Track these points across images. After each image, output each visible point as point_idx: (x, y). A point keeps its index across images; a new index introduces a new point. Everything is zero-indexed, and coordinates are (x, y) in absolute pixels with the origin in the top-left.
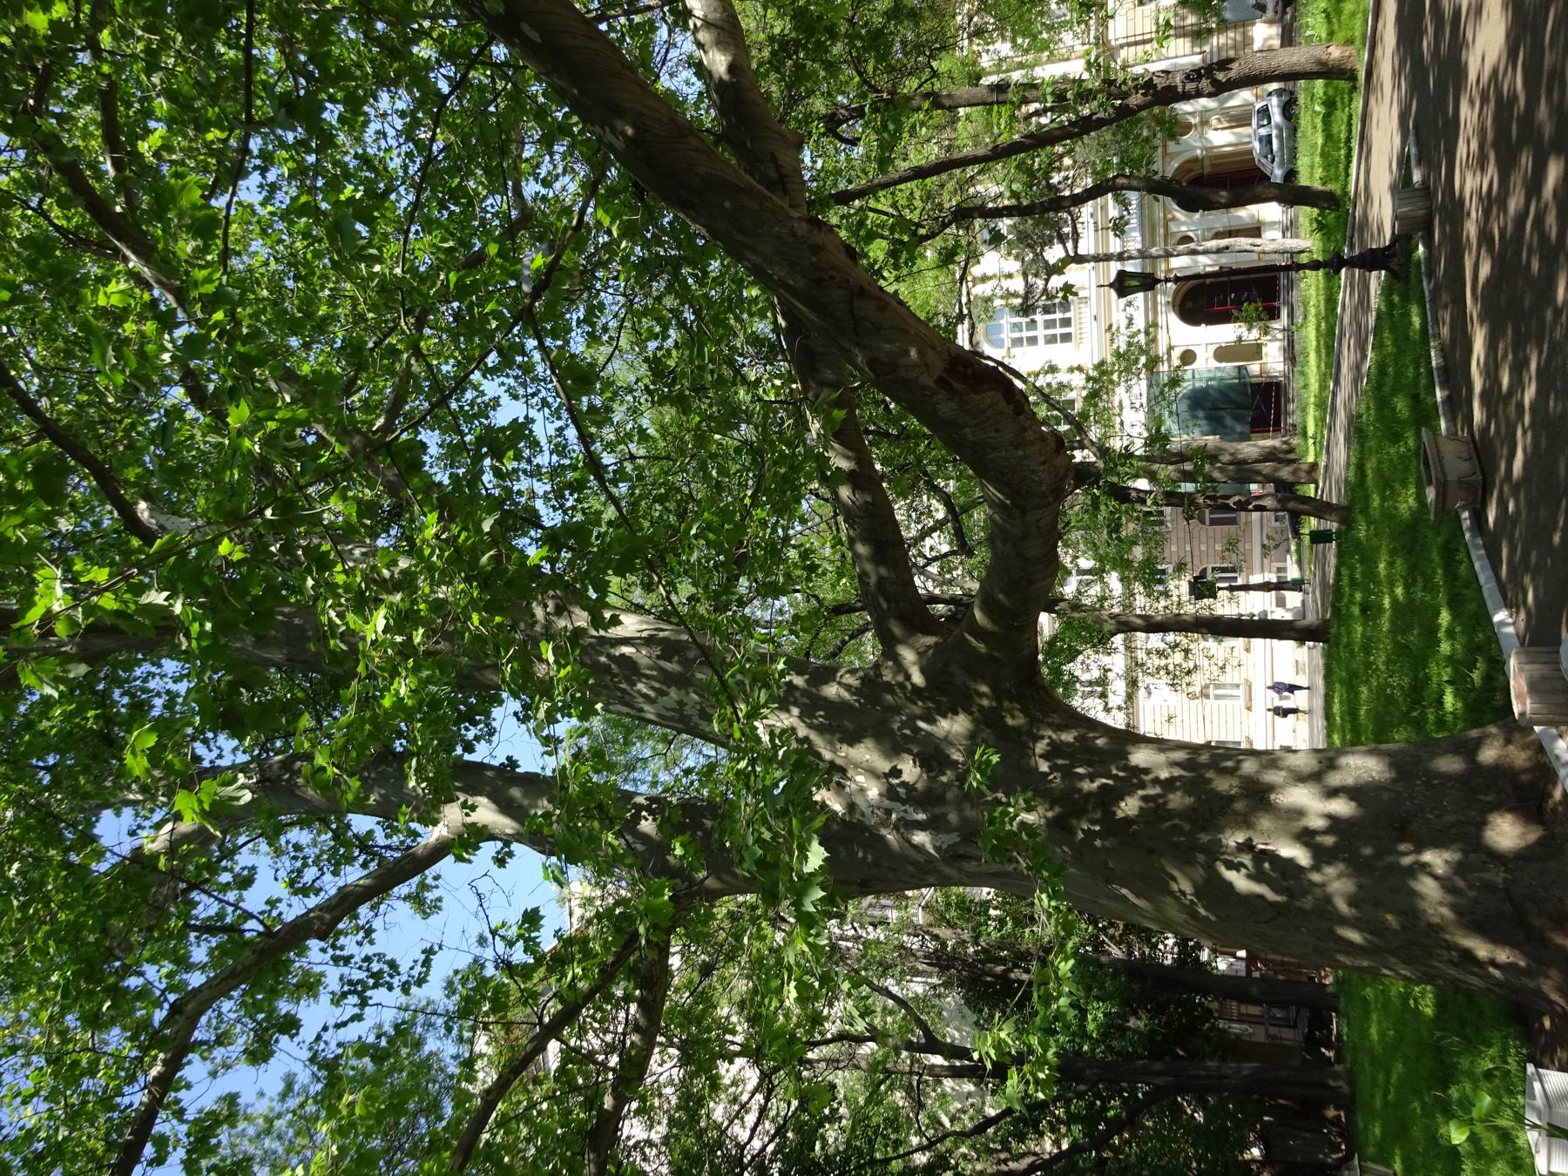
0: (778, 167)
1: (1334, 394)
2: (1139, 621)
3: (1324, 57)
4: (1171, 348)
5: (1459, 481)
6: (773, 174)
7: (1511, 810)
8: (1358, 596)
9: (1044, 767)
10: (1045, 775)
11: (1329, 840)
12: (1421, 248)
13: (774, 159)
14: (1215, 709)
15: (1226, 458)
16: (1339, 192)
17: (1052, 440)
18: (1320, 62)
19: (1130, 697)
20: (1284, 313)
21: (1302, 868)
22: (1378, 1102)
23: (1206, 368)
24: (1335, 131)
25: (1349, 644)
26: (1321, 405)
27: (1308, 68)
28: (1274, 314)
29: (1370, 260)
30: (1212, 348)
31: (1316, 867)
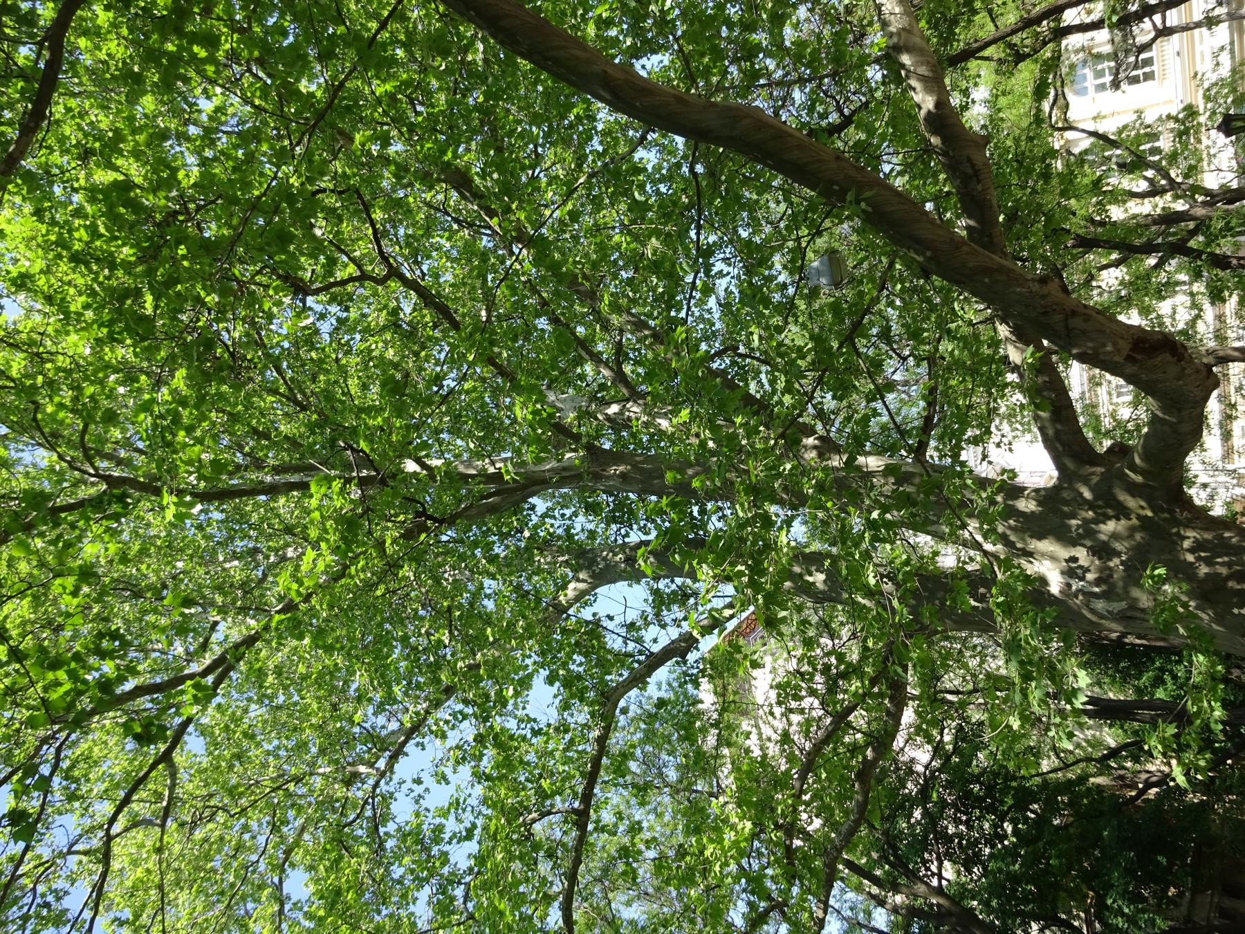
0: (973, 166)
2: (1236, 354)
6: (970, 171)
9: (1190, 558)
13: (969, 160)
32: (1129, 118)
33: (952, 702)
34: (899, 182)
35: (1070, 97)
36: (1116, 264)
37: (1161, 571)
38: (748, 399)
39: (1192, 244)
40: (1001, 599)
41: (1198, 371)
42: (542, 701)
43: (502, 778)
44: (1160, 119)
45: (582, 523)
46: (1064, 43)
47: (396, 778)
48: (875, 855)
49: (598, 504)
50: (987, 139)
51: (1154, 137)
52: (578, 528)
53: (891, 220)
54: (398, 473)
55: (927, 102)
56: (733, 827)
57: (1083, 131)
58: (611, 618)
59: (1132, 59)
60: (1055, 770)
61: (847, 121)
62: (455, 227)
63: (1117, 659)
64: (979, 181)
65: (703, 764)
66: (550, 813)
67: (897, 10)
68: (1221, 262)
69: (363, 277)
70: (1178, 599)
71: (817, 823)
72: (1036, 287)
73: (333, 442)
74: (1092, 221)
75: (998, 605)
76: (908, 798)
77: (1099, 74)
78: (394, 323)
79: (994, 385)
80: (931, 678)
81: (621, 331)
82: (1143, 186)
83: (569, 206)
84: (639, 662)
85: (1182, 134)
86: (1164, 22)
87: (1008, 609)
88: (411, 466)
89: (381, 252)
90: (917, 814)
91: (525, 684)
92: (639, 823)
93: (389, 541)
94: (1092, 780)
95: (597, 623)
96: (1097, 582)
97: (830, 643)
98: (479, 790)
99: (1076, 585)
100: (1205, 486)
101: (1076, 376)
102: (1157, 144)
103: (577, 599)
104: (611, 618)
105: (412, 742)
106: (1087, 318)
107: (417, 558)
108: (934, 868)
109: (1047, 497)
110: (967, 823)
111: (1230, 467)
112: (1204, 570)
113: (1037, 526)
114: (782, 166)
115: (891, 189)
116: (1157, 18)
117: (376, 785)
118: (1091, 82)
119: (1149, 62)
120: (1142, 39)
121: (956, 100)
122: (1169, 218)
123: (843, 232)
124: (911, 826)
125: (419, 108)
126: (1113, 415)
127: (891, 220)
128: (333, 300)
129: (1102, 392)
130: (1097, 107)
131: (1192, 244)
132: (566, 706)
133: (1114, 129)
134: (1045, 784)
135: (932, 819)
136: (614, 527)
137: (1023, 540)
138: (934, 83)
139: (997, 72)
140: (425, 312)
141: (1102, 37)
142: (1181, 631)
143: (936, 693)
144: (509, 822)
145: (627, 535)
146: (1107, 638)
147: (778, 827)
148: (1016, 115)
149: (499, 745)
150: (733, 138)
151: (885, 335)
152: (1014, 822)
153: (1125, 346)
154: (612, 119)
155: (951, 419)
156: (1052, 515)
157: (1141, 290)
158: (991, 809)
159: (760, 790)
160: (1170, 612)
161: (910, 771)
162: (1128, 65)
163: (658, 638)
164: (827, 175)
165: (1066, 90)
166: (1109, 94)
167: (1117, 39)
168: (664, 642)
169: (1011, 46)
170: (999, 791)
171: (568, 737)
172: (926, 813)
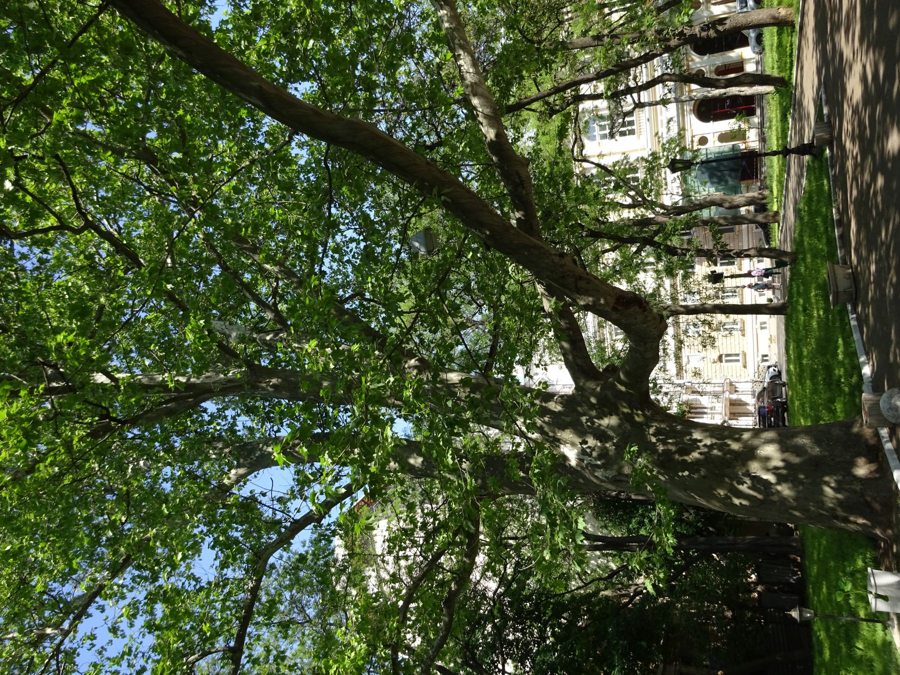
0: (520, 177)
1: (787, 180)
2: (682, 309)
3: (777, 15)
4: (693, 137)
5: (844, 291)
6: (518, 181)
7: (864, 456)
8: (801, 301)
9: (654, 440)
10: (655, 443)
11: (784, 472)
12: (828, 151)
13: (518, 174)
14: (726, 368)
15: (727, 205)
16: (787, 78)
17: (658, 317)
18: (774, 18)
19: (679, 349)
20: (758, 112)
21: (772, 484)
22: (816, 557)
23: (714, 147)
24: (784, 43)
25: (796, 323)
26: (780, 182)
27: (768, 21)
28: (752, 113)
29: (802, 150)
30: (717, 135)
31: (778, 483)
32: (619, 157)
33: (511, 545)
34: (475, 185)
35: (586, 141)
36: (613, 249)
37: (635, 448)
38: (368, 330)
39: (656, 239)
40: (537, 471)
41: (655, 319)
42: (206, 564)
43: (168, 628)
44: (637, 160)
45: (244, 421)
46: (581, 107)
47: (79, 636)
48: (459, 661)
49: (257, 407)
50: (532, 160)
51: (634, 170)
52: (240, 427)
53: (464, 208)
54: (85, 383)
55: (490, 134)
56: (353, 649)
57: (592, 163)
58: (264, 495)
59: (620, 121)
60: (579, 588)
61: (440, 143)
62: (148, 193)
63: (617, 508)
64: (524, 188)
65: (334, 602)
66: (210, 653)
67: (471, 70)
68: (672, 251)
69: (62, 227)
70: (647, 467)
71: (419, 640)
72: (557, 259)
73: (32, 357)
74: (598, 220)
75: (535, 475)
76: (482, 617)
77: (602, 128)
78: (92, 267)
79: (532, 325)
80: (497, 531)
81: (277, 280)
82: (629, 201)
83: (234, 182)
84: (285, 527)
85: (650, 170)
86: (639, 99)
87: (542, 477)
88: (100, 378)
89: (79, 207)
90: (489, 628)
91: (196, 548)
92: (283, 652)
93: (76, 439)
94: (603, 593)
95: (253, 499)
96: (599, 457)
97: (429, 506)
98: (150, 640)
99: (587, 460)
100: (666, 394)
101: (590, 321)
102: (637, 175)
103: (237, 481)
104: (264, 495)
105: (94, 605)
106: (589, 282)
107: (102, 453)
108: (500, 666)
109: (567, 400)
110: (522, 631)
111: (681, 382)
112: (661, 448)
113: (559, 422)
114: (391, 167)
115: (468, 191)
116: (635, 95)
117: (62, 642)
118: (597, 132)
119: (631, 123)
120: (627, 109)
121: (510, 134)
122: (644, 222)
123: (433, 217)
124: (485, 637)
125: (119, 100)
126: (613, 347)
127: (464, 208)
128: (35, 243)
129: (606, 331)
130: (601, 150)
131: (656, 239)
132: (224, 565)
133: (611, 163)
134: (573, 598)
135: (499, 631)
136: (269, 425)
137: (554, 432)
138: (495, 120)
139: (539, 120)
140: (118, 257)
141: (602, 104)
142: (649, 488)
143: (502, 539)
144: (174, 662)
145: (279, 431)
146: (609, 496)
147: (386, 646)
148: (548, 150)
149: (167, 600)
150: (355, 146)
151: (467, 289)
152: (552, 627)
153: (612, 301)
154: (275, 124)
155: (506, 348)
156: (571, 414)
157: (629, 267)
158: (538, 619)
159: (379, 622)
160: (641, 479)
161: (484, 597)
162: (619, 124)
163: (300, 508)
164: (425, 177)
165: (583, 137)
166: (607, 141)
167: (612, 107)
168: (304, 511)
169: (548, 103)
170: (547, 606)
171: (226, 590)
172: (495, 626)
